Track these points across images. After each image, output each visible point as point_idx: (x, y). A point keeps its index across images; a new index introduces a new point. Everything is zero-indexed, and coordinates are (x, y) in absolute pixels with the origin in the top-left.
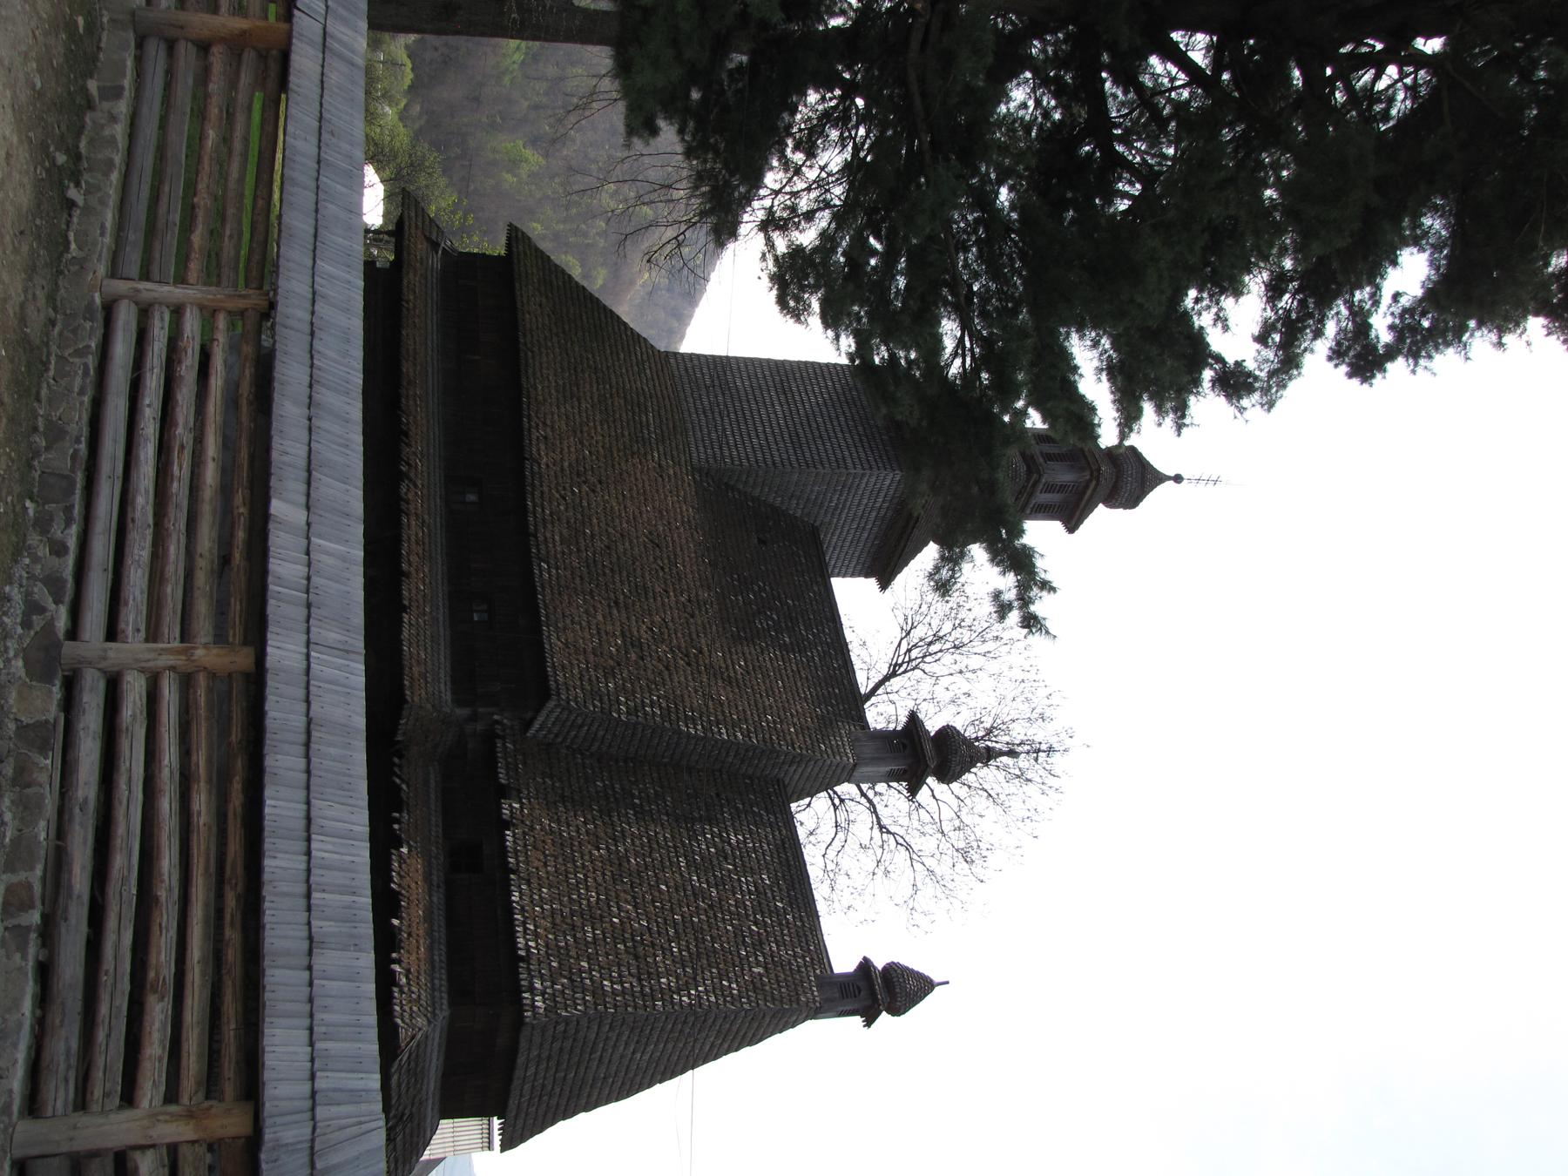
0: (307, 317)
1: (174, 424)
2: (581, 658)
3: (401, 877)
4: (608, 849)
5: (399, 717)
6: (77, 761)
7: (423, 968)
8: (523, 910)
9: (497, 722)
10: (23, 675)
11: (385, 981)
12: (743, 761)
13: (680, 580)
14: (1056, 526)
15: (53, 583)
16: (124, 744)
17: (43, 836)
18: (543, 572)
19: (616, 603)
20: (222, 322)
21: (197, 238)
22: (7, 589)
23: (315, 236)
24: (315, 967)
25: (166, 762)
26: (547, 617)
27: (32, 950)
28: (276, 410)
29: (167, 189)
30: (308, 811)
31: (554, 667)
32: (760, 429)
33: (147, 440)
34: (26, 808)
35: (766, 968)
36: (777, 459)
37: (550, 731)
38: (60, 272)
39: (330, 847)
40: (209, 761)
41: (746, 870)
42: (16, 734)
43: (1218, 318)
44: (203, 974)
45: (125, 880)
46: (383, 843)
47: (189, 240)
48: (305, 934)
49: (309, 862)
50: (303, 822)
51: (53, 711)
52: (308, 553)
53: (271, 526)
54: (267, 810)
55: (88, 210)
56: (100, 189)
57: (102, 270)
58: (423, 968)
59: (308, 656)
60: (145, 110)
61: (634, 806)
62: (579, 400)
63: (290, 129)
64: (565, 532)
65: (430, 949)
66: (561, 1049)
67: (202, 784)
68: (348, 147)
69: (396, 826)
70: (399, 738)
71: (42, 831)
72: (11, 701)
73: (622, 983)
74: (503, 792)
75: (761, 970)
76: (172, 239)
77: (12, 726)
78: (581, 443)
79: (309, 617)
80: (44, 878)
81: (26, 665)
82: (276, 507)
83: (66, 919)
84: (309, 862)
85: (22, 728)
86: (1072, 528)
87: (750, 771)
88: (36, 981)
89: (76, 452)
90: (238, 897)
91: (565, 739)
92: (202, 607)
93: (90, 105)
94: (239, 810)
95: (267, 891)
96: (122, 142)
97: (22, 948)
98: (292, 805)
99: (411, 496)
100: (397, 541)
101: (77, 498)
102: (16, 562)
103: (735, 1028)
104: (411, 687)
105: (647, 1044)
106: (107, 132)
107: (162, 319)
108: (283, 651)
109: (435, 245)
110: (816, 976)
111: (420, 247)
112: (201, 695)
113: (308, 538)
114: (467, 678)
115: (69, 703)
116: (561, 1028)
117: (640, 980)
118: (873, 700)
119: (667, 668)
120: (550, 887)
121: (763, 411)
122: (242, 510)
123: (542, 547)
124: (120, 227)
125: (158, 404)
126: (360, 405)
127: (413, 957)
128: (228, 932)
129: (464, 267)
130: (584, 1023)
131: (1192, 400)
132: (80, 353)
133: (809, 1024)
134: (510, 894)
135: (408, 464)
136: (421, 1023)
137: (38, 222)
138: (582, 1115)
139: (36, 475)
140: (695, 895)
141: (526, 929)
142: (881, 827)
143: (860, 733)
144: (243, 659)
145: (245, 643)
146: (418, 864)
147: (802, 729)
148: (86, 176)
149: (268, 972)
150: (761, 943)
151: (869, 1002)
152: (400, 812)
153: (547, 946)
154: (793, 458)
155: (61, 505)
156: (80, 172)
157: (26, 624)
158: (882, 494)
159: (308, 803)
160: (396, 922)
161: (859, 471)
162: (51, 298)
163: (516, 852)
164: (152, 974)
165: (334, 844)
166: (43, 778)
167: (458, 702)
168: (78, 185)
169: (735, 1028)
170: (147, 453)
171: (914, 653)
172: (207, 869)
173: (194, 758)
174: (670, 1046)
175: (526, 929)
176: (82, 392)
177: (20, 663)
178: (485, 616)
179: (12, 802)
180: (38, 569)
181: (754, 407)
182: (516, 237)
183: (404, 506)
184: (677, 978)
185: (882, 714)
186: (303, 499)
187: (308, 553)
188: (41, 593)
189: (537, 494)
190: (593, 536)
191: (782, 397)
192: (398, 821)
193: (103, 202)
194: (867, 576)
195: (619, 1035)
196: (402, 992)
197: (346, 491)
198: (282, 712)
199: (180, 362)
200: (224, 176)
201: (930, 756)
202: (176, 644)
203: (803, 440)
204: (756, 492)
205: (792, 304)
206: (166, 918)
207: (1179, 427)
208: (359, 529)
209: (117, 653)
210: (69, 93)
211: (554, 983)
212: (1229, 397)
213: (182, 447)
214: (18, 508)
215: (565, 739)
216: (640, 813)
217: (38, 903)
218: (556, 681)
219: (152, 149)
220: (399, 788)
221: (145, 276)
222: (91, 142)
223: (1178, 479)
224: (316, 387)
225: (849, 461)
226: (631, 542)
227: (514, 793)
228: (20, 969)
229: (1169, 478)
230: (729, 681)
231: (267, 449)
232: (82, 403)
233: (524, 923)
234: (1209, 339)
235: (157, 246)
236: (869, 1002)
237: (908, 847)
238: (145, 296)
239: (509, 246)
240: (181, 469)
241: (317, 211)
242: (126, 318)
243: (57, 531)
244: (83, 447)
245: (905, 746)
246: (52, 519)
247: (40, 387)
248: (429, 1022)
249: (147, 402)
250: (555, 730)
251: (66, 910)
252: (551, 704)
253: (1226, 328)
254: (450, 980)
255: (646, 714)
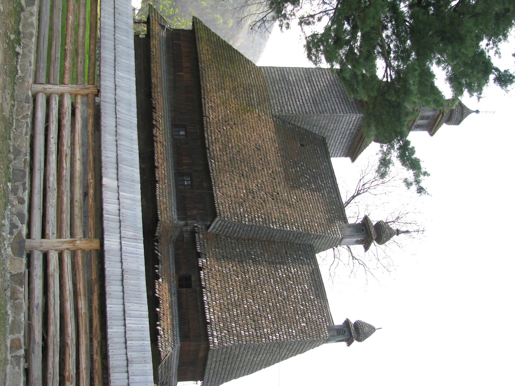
0: (113, 96)
1: (63, 145)
2: (229, 199)
3: (160, 291)
4: (242, 277)
5: (156, 226)
6: (34, 288)
7: (169, 327)
8: (208, 303)
9: (196, 227)
10: (11, 254)
11: (154, 334)
12: (296, 238)
13: (268, 164)
14: (425, 134)
15: (20, 215)
16: (51, 280)
17: (23, 319)
18: (213, 164)
19: (243, 175)
20: (79, 100)
21: (67, 64)
22: (3, 222)
23: (115, 60)
24: (129, 372)
25: (68, 288)
26: (215, 183)
27: (22, 365)
28: (103, 139)
29: (54, 43)
30: (124, 308)
31: (218, 203)
32: (300, 98)
33: (52, 153)
34: (16, 308)
35: (307, 324)
36: (307, 110)
37: (217, 230)
38: (15, 83)
39: (133, 322)
40: (84, 287)
41: (299, 283)
42: (11, 278)
43: (496, 52)
44: (87, 374)
45: (54, 336)
46: (151, 278)
47: (65, 65)
48: (125, 358)
49: (125, 329)
50: (122, 312)
51: (23, 269)
52: (119, 199)
53: (104, 189)
54: (108, 309)
55: (24, 55)
56: (28, 46)
57: (31, 80)
58: (169, 327)
59: (121, 243)
60: (44, 9)
61: (252, 259)
62: (224, 89)
63: (103, 6)
64: (221, 146)
65: (172, 320)
66: (225, 358)
67: (82, 296)
68: (126, 19)
69: (157, 271)
70: (157, 235)
71: (22, 317)
72: (8, 265)
73: (248, 332)
74: (199, 255)
75: (305, 324)
76: (57, 65)
77: (9, 275)
78: (226, 108)
79: (120, 226)
80: (24, 336)
81: (12, 250)
82: (105, 181)
83: (34, 353)
84: (125, 329)
85: (12, 276)
86: (432, 135)
87: (299, 242)
88: (24, 376)
89: (25, 159)
90: (98, 342)
91: (224, 232)
92: (78, 223)
93: (22, 10)
94: (97, 307)
95: (109, 342)
96: (36, 23)
97: (18, 364)
98: (118, 306)
99: (158, 134)
100: (153, 153)
101: (27, 180)
102: (5, 209)
103: (294, 348)
104: (161, 214)
105: (259, 355)
106: (30, 21)
107: (56, 100)
108: (111, 242)
109: (163, 27)
110: (327, 326)
111: (156, 28)
112: (80, 259)
113: (118, 193)
114: (183, 209)
115: (29, 265)
116: (224, 350)
117: (256, 330)
118: (349, 205)
119: (264, 202)
120: (219, 293)
121: (301, 90)
122: (91, 181)
123: (212, 153)
124: (37, 61)
125: (56, 137)
126: (137, 132)
127: (166, 323)
128: (95, 357)
129: (176, 35)
130: (234, 348)
131: (484, 88)
132: (25, 117)
133: (325, 345)
134: (203, 297)
135: (156, 121)
136: (169, 348)
137: (5, 67)
138: (234, 380)
139: (11, 170)
140: (277, 294)
141: (210, 311)
142: (353, 257)
143: (344, 225)
144: (95, 244)
145: (95, 237)
146: (166, 286)
147: (320, 224)
148: (23, 41)
149: (112, 375)
150: (305, 313)
151: (348, 337)
152: (158, 264)
153: (218, 318)
154: (314, 109)
155: (21, 183)
156: (20, 40)
157: (11, 233)
158: (352, 123)
159: (124, 305)
160: (158, 309)
161: (342, 114)
162: (13, 97)
163: (205, 280)
164: (67, 374)
165: (134, 320)
166: (21, 296)
167: (180, 219)
168: (20, 45)
169: (294, 348)
170: (53, 158)
171: (366, 186)
172: (86, 331)
173: (78, 286)
174: (268, 355)
175: (210, 311)
176: (26, 134)
177: (10, 249)
178: (190, 182)
179: (11, 306)
180: (14, 210)
181: (297, 88)
182: (195, 21)
183: (155, 139)
184: (271, 329)
185: (353, 214)
186: (115, 176)
187: (119, 199)
188: (16, 220)
189: (209, 131)
190: (232, 147)
191: (309, 84)
192: (157, 269)
193: (30, 51)
194: (346, 157)
195: (248, 352)
196: (161, 337)
197: (133, 171)
198: (112, 268)
199: (64, 118)
200: (77, 33)
201: (372, 233)
202: (69, 239)
203: (318, 102)
204: (299, 125)
205: (313, 58)
206: (71, 351)
207: (479, 98)
208: (139, 186)
209: (46, 244)
210: (14, 8)
211: (221, 333)
212: (501, 86)
213: (66, 155)
214: (5, 188)
215: (224, 232)
216: (254, 261)
217: (23, 347)
218: (219, 210)
219: (48, 26)
220: (157, 255)
221: (48, 82)
222: (24, 26)
223: (477, 112)
224: (118, 126)
225: (337, 110)
226: (248, 149)
227: (203, 255)
228: (18, 373)
229: (474, 112)
230: (290, 206)
231: (100, 151)
232: (26, 139)
233: (209, 309)
234: (492, 61)
235: (52, 68)
236: (348, 337)
237: (364, 265)
238: (49, 91)
239: (193, 25)
240: (66, 165)
241: (115, 49)
242: (41, 100)
243: (20, 193)
244: (28, 157)
245: (363, 230)
246: (18, 189)
247: (10, 133)
248: (172, 349)
249: (52, 136)
250: (219, 229)
251: (33, 348)
252: (217, 219)
253: (500, 57)
254: (180, 331)
255: (256, 221)
